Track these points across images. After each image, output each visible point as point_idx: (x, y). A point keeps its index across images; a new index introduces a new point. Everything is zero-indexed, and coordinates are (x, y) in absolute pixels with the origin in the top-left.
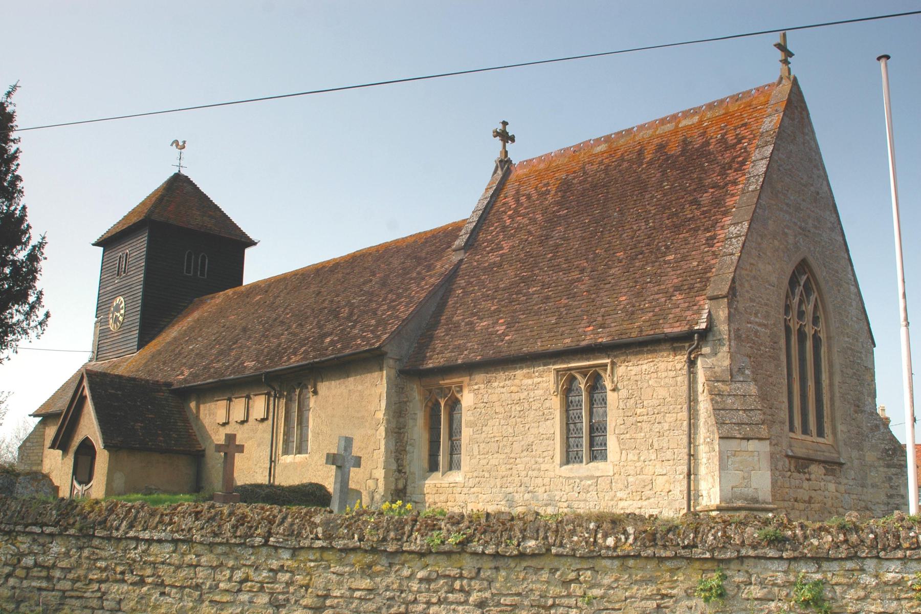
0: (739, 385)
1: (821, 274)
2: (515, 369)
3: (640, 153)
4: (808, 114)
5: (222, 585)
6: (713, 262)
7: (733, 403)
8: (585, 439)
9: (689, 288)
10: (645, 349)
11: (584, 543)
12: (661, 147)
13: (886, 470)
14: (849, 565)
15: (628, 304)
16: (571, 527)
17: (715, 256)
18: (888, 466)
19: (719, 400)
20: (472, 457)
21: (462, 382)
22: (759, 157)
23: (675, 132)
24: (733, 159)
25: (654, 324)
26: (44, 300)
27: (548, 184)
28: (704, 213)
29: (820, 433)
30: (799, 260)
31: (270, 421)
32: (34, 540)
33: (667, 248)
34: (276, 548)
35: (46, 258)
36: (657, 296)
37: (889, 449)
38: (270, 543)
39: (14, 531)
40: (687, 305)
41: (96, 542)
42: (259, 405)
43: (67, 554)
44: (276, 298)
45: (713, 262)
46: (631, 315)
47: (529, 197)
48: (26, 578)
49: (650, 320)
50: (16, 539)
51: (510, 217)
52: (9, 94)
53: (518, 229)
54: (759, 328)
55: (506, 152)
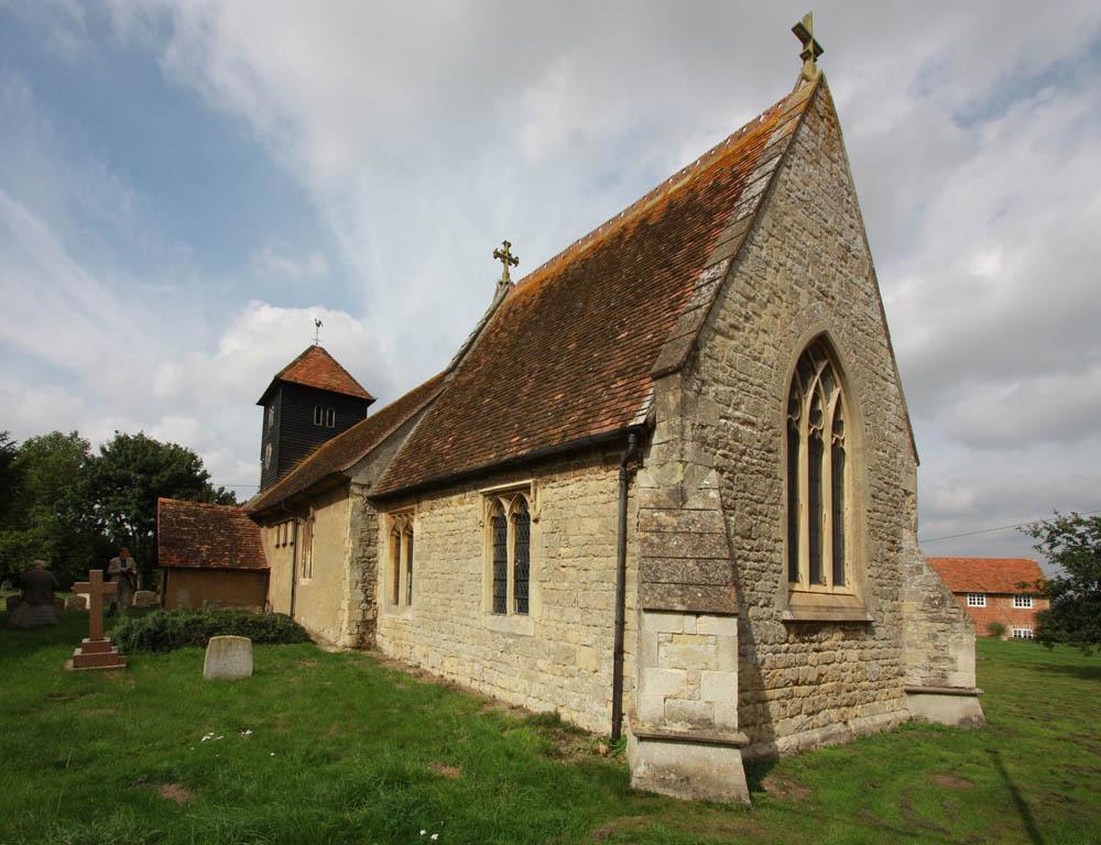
0: (694, 515)
1: (848, 360)
2: (451, 495)
4: (840, 134)
13: (929, 624)
18: (933, 620)
19: (656, 541)
21: (527, 488)
37: (934, 599)
54: (742, 428)
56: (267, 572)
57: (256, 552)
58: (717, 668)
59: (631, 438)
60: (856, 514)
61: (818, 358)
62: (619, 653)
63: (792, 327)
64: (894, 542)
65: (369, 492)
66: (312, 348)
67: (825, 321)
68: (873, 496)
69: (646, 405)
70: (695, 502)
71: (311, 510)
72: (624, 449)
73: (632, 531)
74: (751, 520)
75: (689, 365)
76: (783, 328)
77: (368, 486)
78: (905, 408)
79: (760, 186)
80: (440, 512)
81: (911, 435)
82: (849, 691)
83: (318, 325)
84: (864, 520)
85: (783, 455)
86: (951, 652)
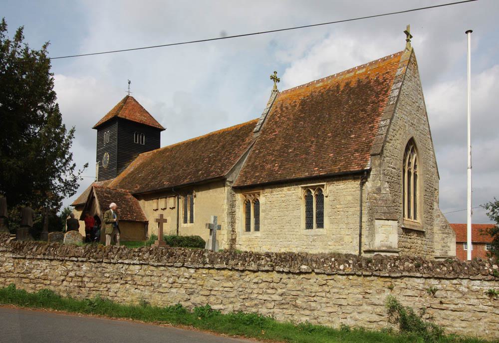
0: (384, 195)
2: (283, 187)
3: (338, 87)
5: (163, 285)
6: (373, 138)
7: (381, 204)
8: (315, 217)
9: (362, 150)
10: (341, 178)
11: (329, 268)
12: (347, 84)
13: (442, 235)
14: (455, 281)
15: (333, 157)
16: (323, 260)
17: (374, 136)
18: (443, 233)
20: (265, 225)
21: (323, 186)
22: (395, 88)
23: (354, 77)
24: (382, 90)
25: (346, 167)
26: (73, 157)
27: (295, 102)
28: (368, 115)
29: (415, 218)
30: (410, 138)
31: (176, 210)
32: (75, 264)
33: (351, 131)
34: (188, 268)
35: (74, 138)
36: (347, 154)
38: (185, 265)
39: (64, 260)
40: (361, 158)
41: (104, 265)
42: (171, 201)
43: (90, 271)
44: (175, 154)
45: (373, 138)
46: (335, 162)
47: (287, 108)
48: (71, 282)
49: (344, 165)
50: (65, 263)
51: (279, 117)
52: (45, 47)
53: (283, 123)
55: (276, 87)
56: (146, 223)
57: (139, 213)
58: (393, 233)
59: (365, 173)
60: (420, 196)
61: (411, 145)
62: (360, 235)
63: (404, 137)
64: (431, 206)
65: (233, 185)
66: (128, 97)
67: (413, 133)
68: (426, 191)
69: (369, 163)
70: (383, 191)
71: (194, 191)
72: (362, 175)
73: (364, 199)
74: (394, 197)
75: (381, 154)
76: (402, 138)
77: (232, 182)
78: (435, 159)
79: (396, 93)
80: (277, 193)
81: (437, 169)
82: (418, 253)
83: (129, 83)
84: (423, 198)
85: (402, 178)
86: (449, 244)
